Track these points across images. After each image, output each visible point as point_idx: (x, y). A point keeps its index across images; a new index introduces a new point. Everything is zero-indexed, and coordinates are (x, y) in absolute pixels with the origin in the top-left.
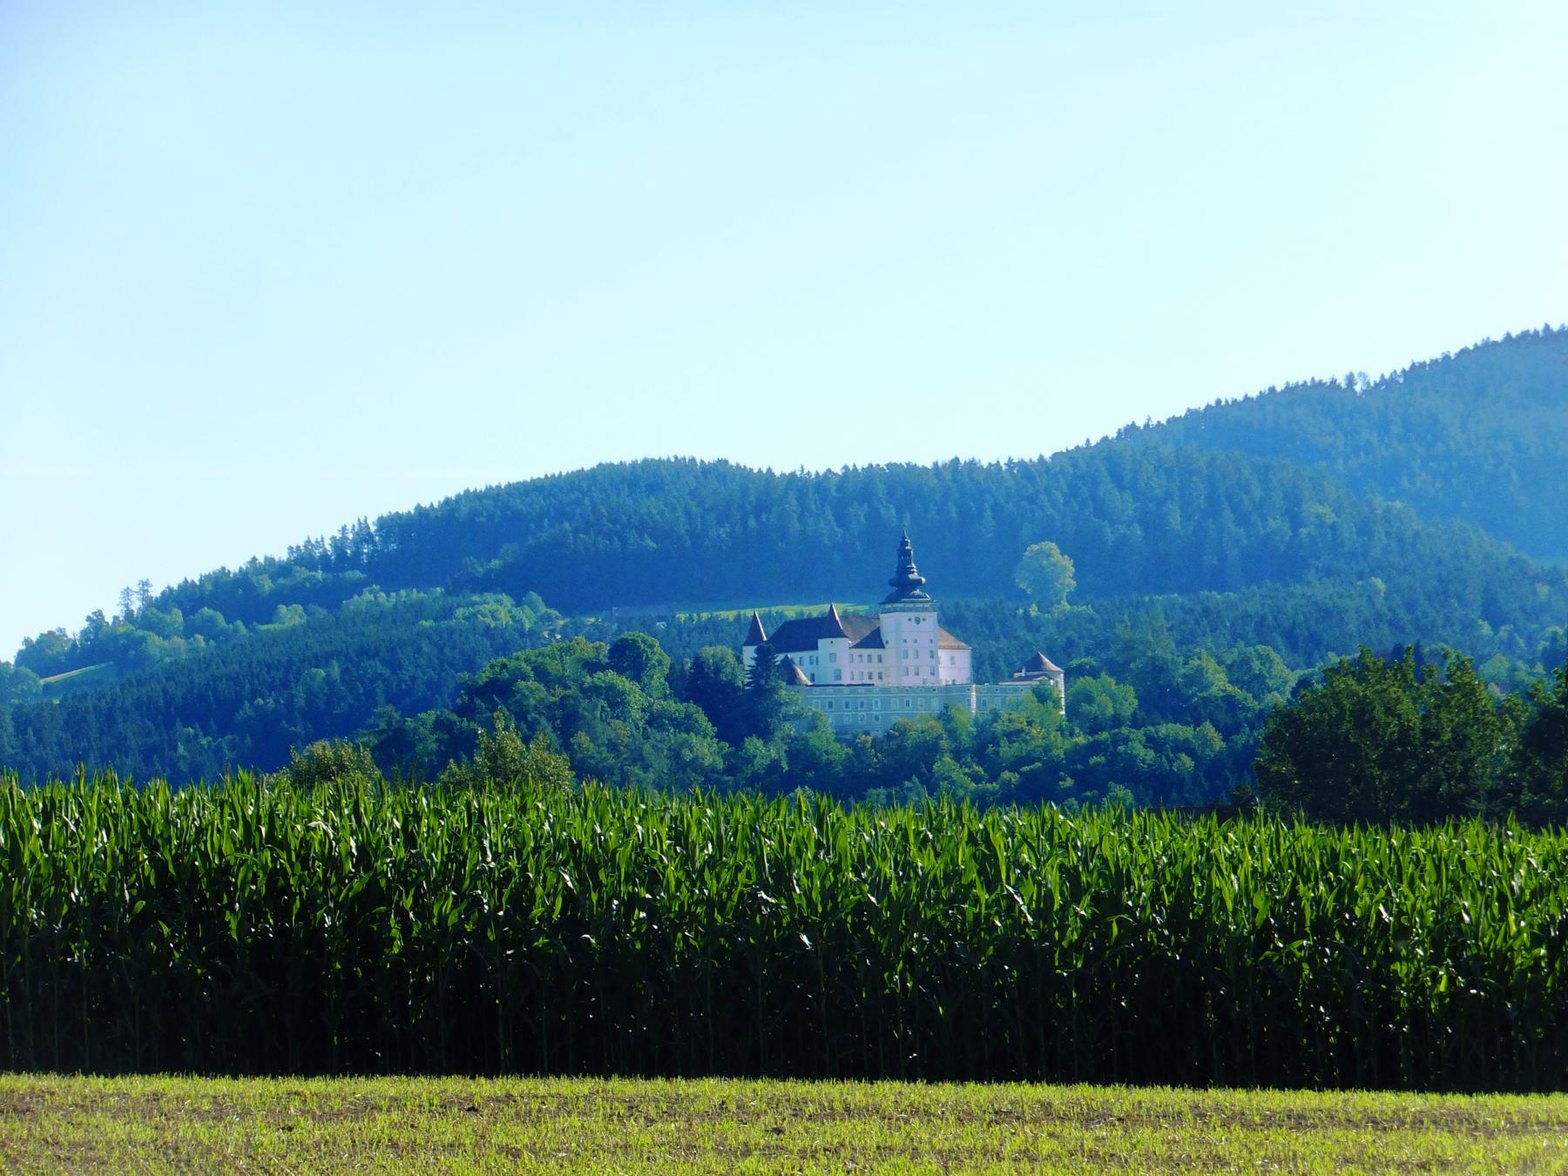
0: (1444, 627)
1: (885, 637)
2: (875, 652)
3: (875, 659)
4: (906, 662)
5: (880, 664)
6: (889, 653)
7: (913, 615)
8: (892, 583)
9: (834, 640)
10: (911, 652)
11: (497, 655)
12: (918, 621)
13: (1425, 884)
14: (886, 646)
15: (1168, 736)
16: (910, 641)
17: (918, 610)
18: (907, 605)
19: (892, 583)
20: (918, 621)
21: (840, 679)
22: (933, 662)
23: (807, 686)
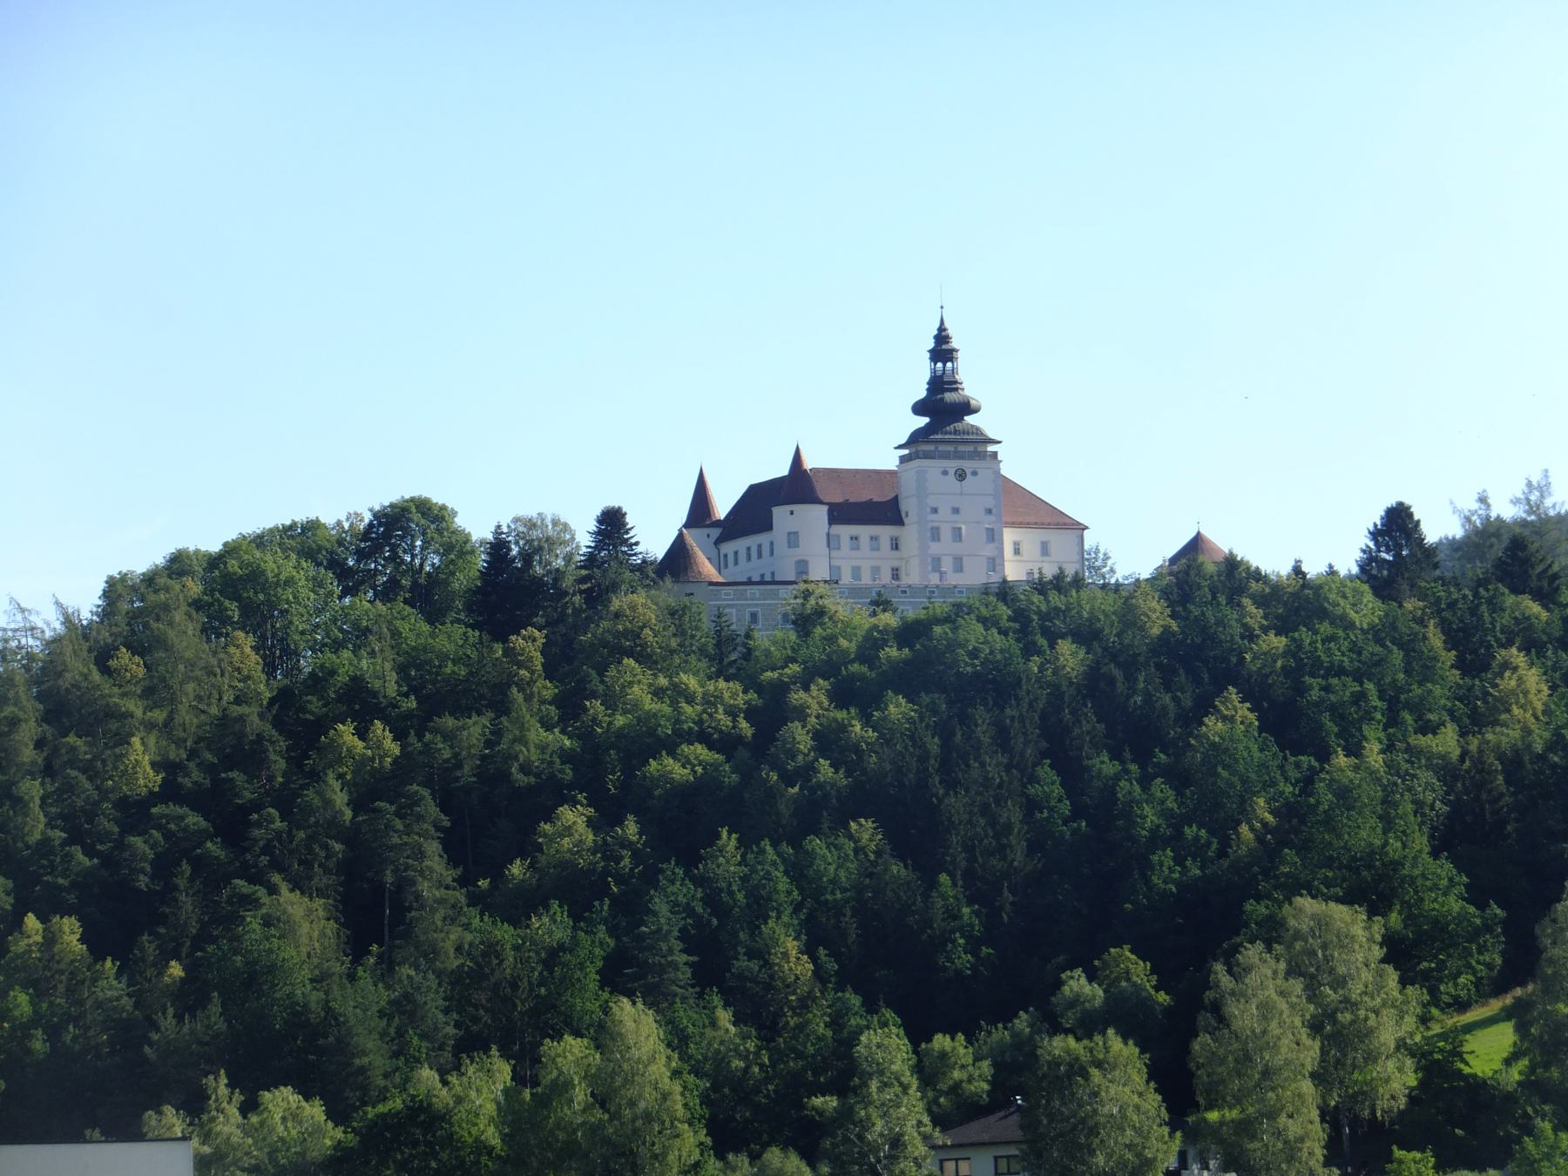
0: (389, 1034)
1: (905, 506)
2: (885, 532)
3: (885, 543)
4: (935, 549)
5: (895, 553)
6: (910, 534)
7: (952, 465)
8: (919, 409)
9: (797, 508)
10: (946, 533)
11: (1452, 641)
12: (961, 475)
13: (1507, 727)
14: (905, 520)
15: (867, 1102)
16: (945, 511)
17: (959, 456)
18: (942, 448)
19: (919, 409)
20: (961, 475)
21: (860, 580)
22: (989, 550)
23: (711, 584)
